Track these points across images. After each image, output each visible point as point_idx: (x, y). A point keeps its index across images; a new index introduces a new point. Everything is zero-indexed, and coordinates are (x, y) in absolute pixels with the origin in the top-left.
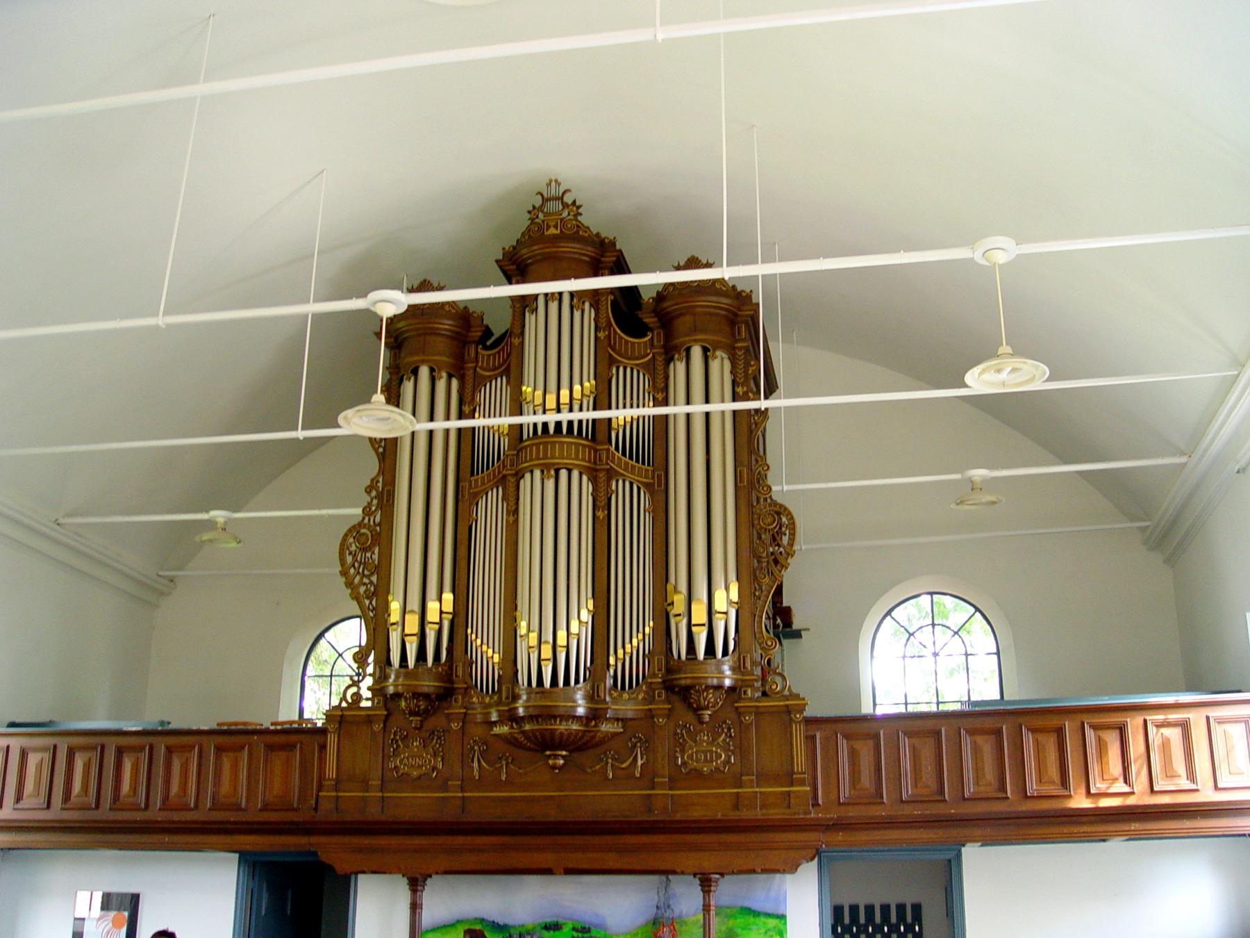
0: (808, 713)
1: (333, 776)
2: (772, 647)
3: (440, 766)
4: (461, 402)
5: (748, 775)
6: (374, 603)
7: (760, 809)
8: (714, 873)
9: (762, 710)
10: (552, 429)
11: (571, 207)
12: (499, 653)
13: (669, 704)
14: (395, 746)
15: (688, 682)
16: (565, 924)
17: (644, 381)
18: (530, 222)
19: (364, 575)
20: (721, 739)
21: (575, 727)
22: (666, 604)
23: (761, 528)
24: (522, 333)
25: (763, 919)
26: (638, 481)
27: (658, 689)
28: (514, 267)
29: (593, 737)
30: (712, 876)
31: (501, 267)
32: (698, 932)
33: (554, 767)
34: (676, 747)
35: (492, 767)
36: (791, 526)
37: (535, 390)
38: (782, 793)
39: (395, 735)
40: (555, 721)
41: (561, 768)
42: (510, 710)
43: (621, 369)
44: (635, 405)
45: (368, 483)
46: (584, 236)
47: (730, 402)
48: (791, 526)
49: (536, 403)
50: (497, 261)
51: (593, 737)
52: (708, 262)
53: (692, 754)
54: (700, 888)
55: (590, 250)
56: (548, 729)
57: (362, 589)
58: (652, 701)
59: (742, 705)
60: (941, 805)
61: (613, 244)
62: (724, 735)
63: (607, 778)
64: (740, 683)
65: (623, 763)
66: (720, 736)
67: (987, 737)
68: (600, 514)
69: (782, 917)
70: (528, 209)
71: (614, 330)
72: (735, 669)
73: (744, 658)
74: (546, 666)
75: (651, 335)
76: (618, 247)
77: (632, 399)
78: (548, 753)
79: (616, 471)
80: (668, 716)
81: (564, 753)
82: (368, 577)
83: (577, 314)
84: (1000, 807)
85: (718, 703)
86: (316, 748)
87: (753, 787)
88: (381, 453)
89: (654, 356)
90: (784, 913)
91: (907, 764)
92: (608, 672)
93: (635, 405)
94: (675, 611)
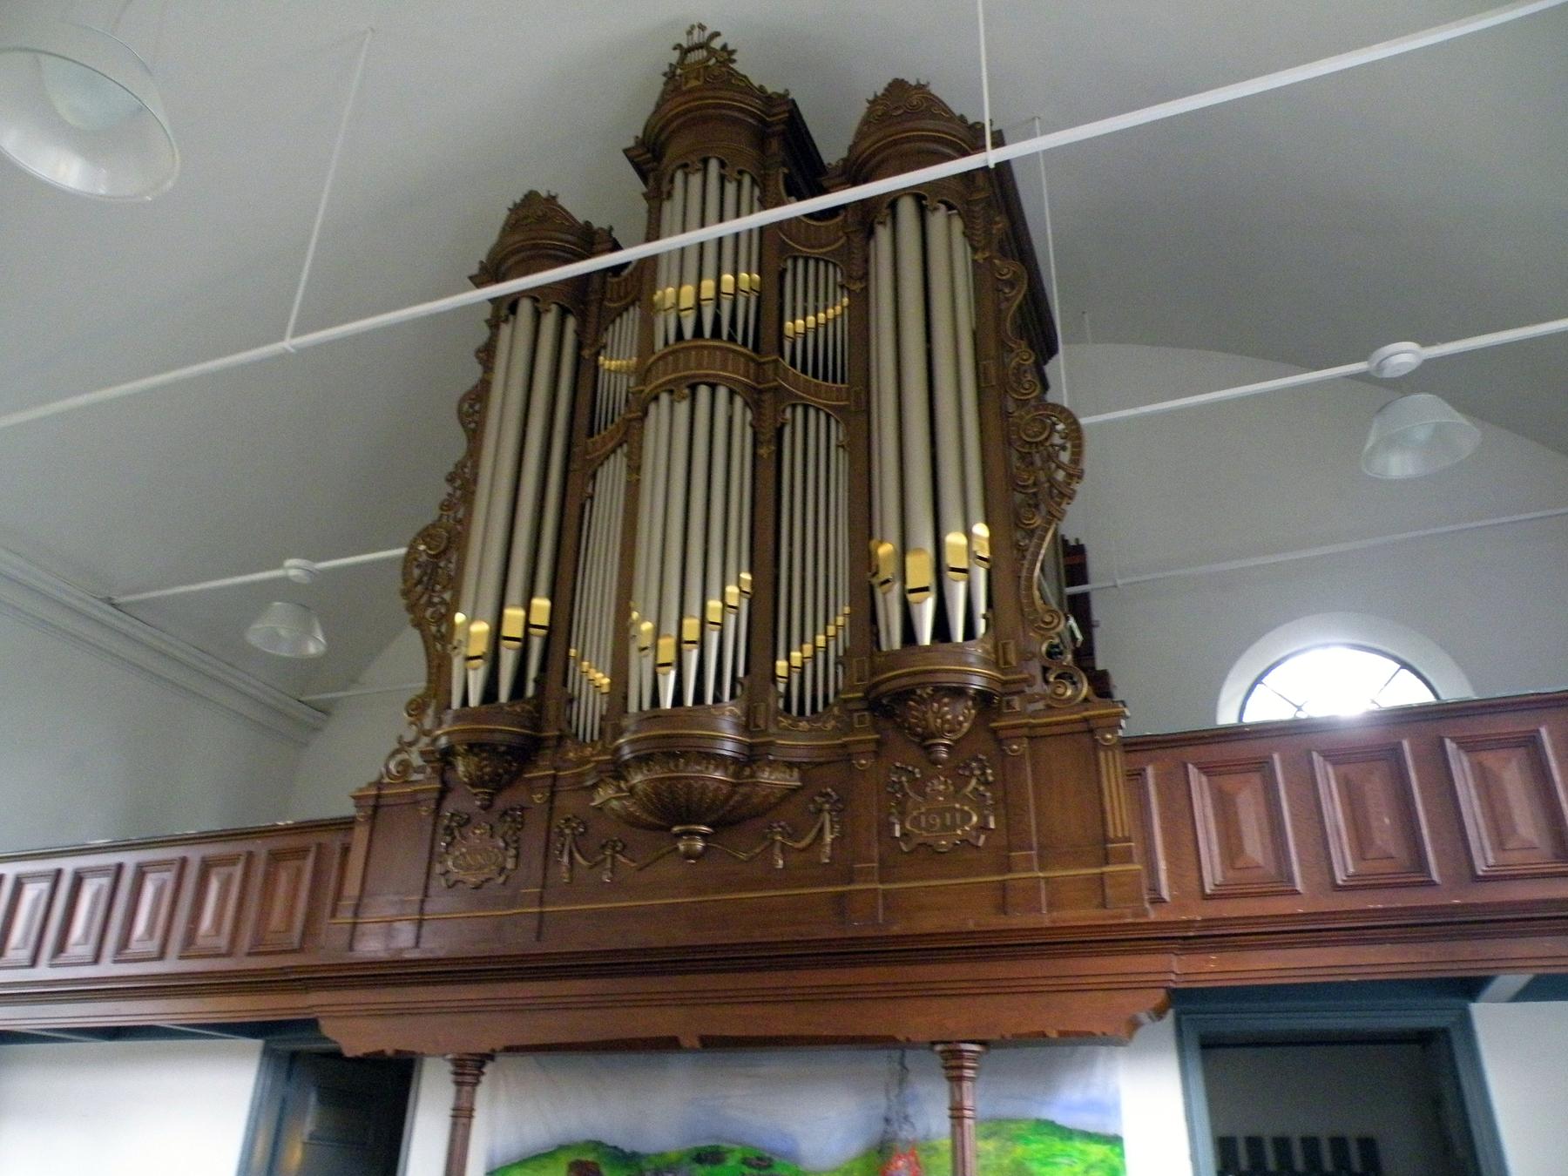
0: (1128, 729)
2: (1053, 625)
5: (1022, 849)
7: (1049, 911)
8: (965, 1042)
9: (1040, 731)
13: (877, 733)
16: (732, 1151)
20: (970, 788)
22: (869, 574)
25: (1078, 1144)
26: (826, 406)
27: (857, 711)
31: (631, 160)
32: (944, 1162)
33: (688, 855)
36: (1075, 435)
38: (1088, 879)
41: (699, 856)
45: (451, 468)
48: (1075, 435)
50: (626, 151)
51: (747, 797)
58: (851, 730)
59: (1003, 724)
60: (1429, 891)
66: (967, 783)
67: (1503, 753)
68: (763, 451)
69: (1115, 1141)
73: (1004, 645)
74: (666, 674)
78: (676, 829)
80: (877, 754)
81: (704, 828)
83: (731, 188)
87: (1032, 870)
90: (1119, 1134)
91: (1335, 813)
92: (772, 686)
94: (883, 575)
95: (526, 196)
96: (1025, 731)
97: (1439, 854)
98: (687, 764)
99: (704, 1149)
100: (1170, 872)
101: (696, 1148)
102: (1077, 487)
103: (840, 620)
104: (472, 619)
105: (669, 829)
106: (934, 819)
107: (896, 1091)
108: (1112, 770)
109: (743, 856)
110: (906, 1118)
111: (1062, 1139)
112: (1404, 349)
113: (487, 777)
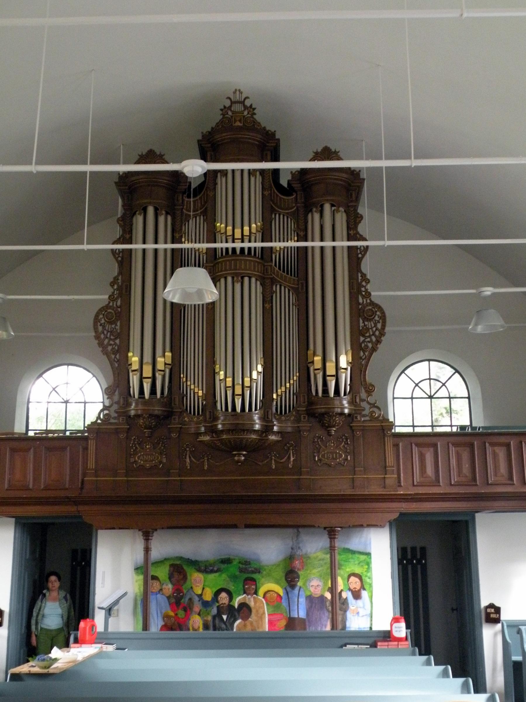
1: (92, 467)
3: (164, 460)
4: (173, 231)
6: (118, 356)
10: (238, 252)
11: (249, 109)
12: (202, 390)
14: (134, 448)
15: (323, 410)
17: (291, 224)
18: (222, 116)
19: (110, 339)
21: (254, 436)
23: (365, 317)
24: (215, 189)
25: (357, 555)
26: (289, 286)
28: (209, 145)
29: (264, 443)
30: (337, 529)
33: (238, 461)
34: (314, 450)
35: (198, 461)
37: (226, 226)
39: (134, 441)
40: (244, 433)
41: (243, 462)
42: (212, 426)
43: (277, 215)
44: (286, 240)
45: (112, 280)
46: (257, 128)
47: (159, 249)
49: (228, 234)
52: (335, 151)
53: (325, 454)
54: (328, 536)
55: (259, 137)
56: (239, 438)
57: (110, 348)
60: (475, 488)
61: (273, 134)
62: (343, 443)
63: (315, 461)
64: (353, 412)
65: (281, 459)
67: (500, 448)
69: (369, 554)
70: (221, 108)
71: (274, 191)
72: (350, 403)
75: (295, 195)
76: (277, 137)
77: (279, 234)
79: (276, 280)
81: (244, 453)
82: (114, 340)
83: (253, 179)
84: (509, 489)
85: (340, 423)
86: (81, 450)
88: (120, 261)
89: (297, 208)
93: (286, 240)
95: (148, 151)
96: (361, 428)
97: (480, 476)
98: (247, 433)
99: (224, 559)
100: (404, 477)
101: (221, 559)
102: (382, 338)
103: (295, 378)
104: (133, 356)
105: (231, 452)
106: (330, 455)
107: (296, 539)
108: (389, 444)
109: (260, 464)
110: (299, 548)
111: (352, 554)
112: (489, 290)
113: (153, 426)
